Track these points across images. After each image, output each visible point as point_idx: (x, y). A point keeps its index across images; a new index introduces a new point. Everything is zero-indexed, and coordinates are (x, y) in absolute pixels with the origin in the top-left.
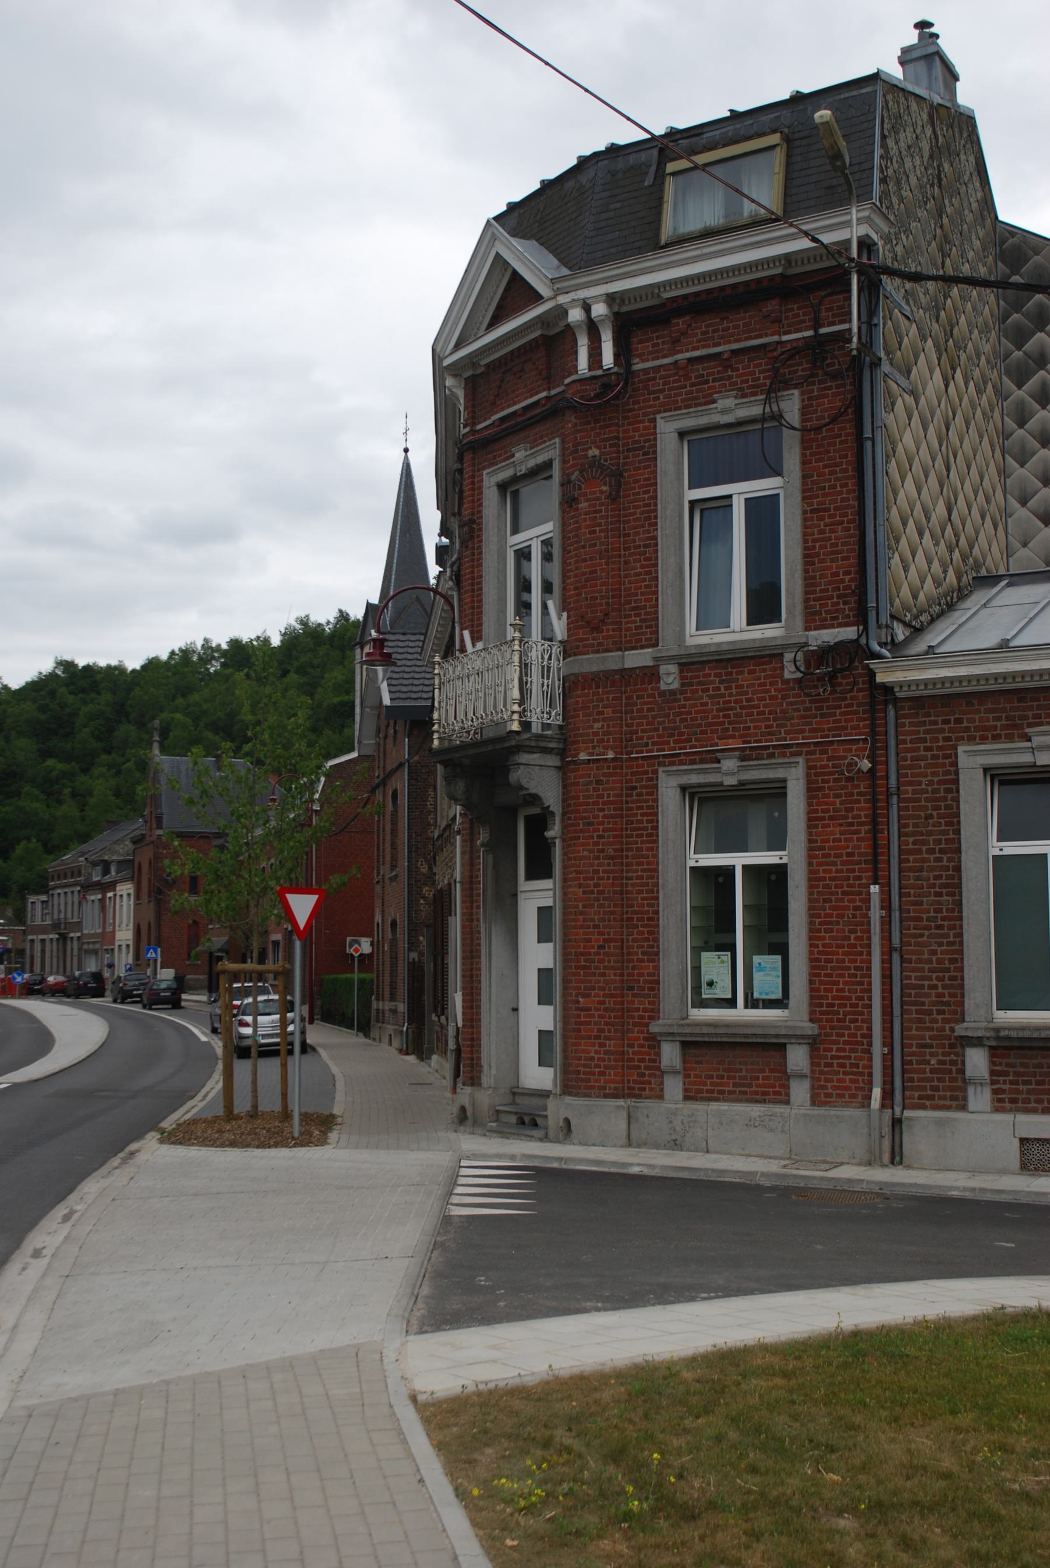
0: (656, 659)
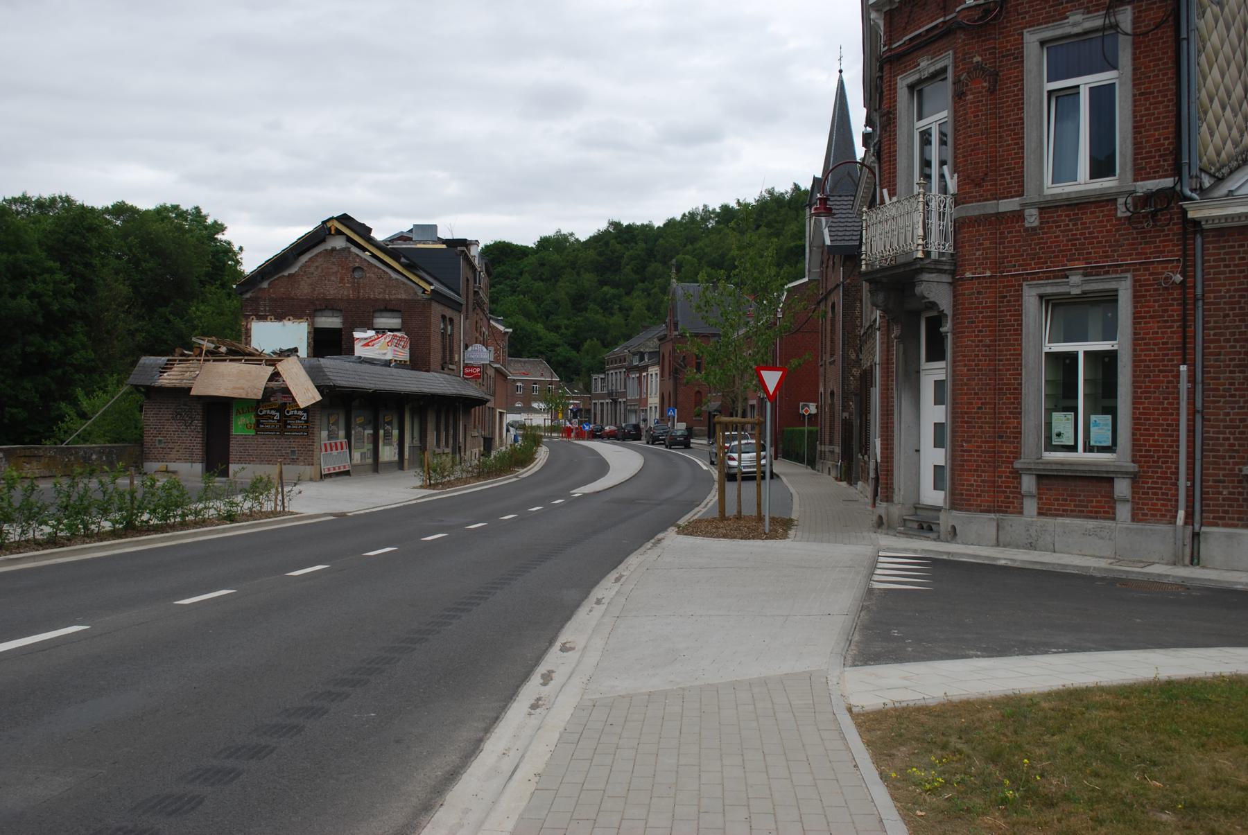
0: (1022, 205)
